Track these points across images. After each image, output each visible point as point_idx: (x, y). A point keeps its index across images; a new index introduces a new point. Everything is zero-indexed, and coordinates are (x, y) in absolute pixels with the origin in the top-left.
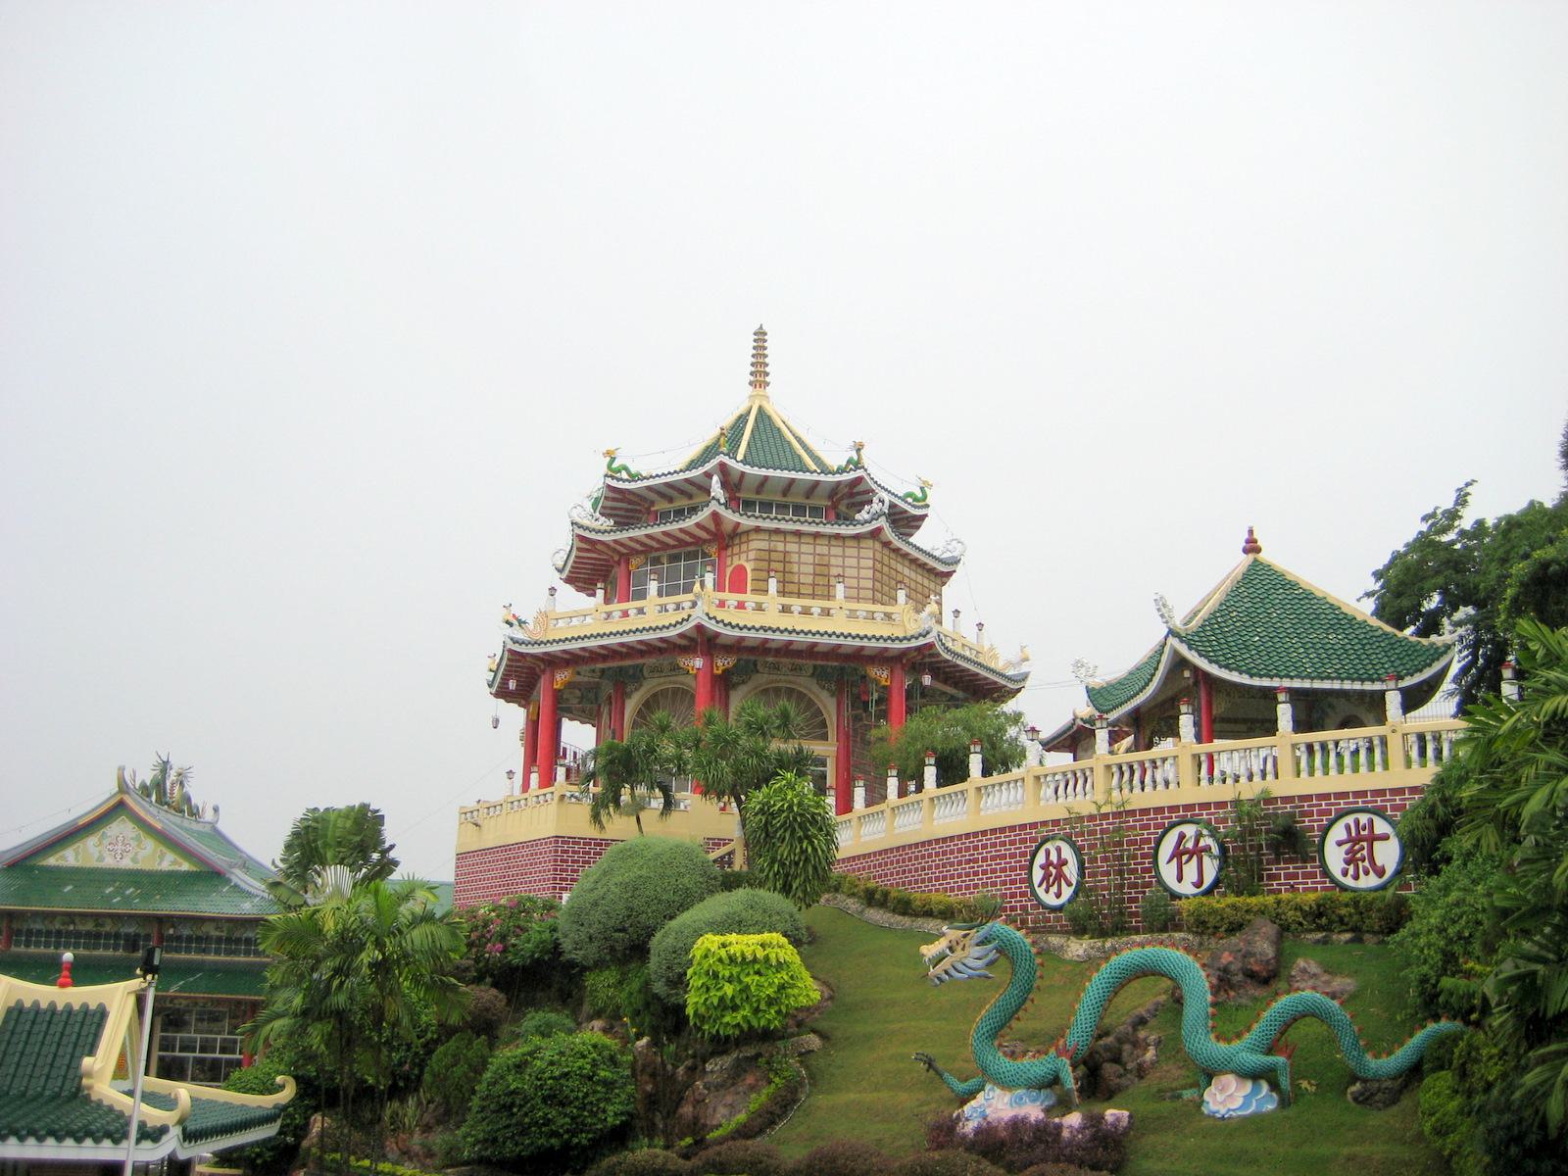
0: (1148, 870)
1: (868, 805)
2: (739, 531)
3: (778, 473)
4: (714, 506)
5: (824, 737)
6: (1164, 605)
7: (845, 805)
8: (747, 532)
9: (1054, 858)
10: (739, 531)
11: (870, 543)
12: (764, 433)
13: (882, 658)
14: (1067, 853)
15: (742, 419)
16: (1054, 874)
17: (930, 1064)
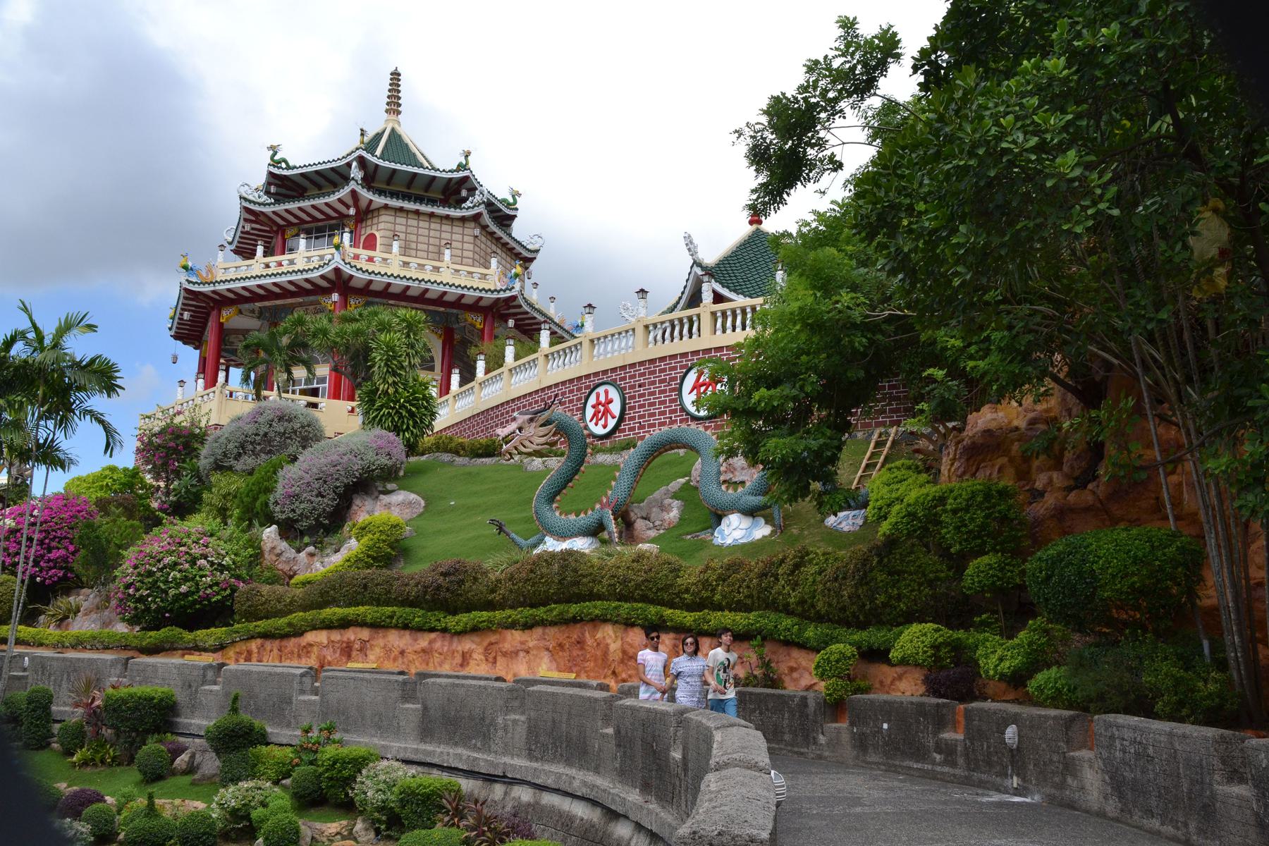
0: (675, 400)
1: (461, 386)
2: (373, 207)
3: (404, 168)
4: (352, 185)
5: (432, 369)
6: (691, 242)
7: (445, 389)
8: (378, 209)
9: (602, 399)
10: (373, 207)
11: (473, 224)
12: (397, 146)
13: (475, 306)
14: (614, 394)
15: (378, 136)
16: (602, 411)
17: (501, 529)
